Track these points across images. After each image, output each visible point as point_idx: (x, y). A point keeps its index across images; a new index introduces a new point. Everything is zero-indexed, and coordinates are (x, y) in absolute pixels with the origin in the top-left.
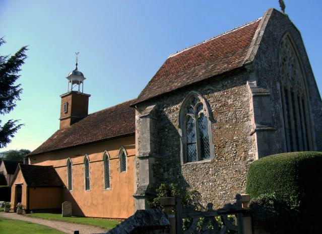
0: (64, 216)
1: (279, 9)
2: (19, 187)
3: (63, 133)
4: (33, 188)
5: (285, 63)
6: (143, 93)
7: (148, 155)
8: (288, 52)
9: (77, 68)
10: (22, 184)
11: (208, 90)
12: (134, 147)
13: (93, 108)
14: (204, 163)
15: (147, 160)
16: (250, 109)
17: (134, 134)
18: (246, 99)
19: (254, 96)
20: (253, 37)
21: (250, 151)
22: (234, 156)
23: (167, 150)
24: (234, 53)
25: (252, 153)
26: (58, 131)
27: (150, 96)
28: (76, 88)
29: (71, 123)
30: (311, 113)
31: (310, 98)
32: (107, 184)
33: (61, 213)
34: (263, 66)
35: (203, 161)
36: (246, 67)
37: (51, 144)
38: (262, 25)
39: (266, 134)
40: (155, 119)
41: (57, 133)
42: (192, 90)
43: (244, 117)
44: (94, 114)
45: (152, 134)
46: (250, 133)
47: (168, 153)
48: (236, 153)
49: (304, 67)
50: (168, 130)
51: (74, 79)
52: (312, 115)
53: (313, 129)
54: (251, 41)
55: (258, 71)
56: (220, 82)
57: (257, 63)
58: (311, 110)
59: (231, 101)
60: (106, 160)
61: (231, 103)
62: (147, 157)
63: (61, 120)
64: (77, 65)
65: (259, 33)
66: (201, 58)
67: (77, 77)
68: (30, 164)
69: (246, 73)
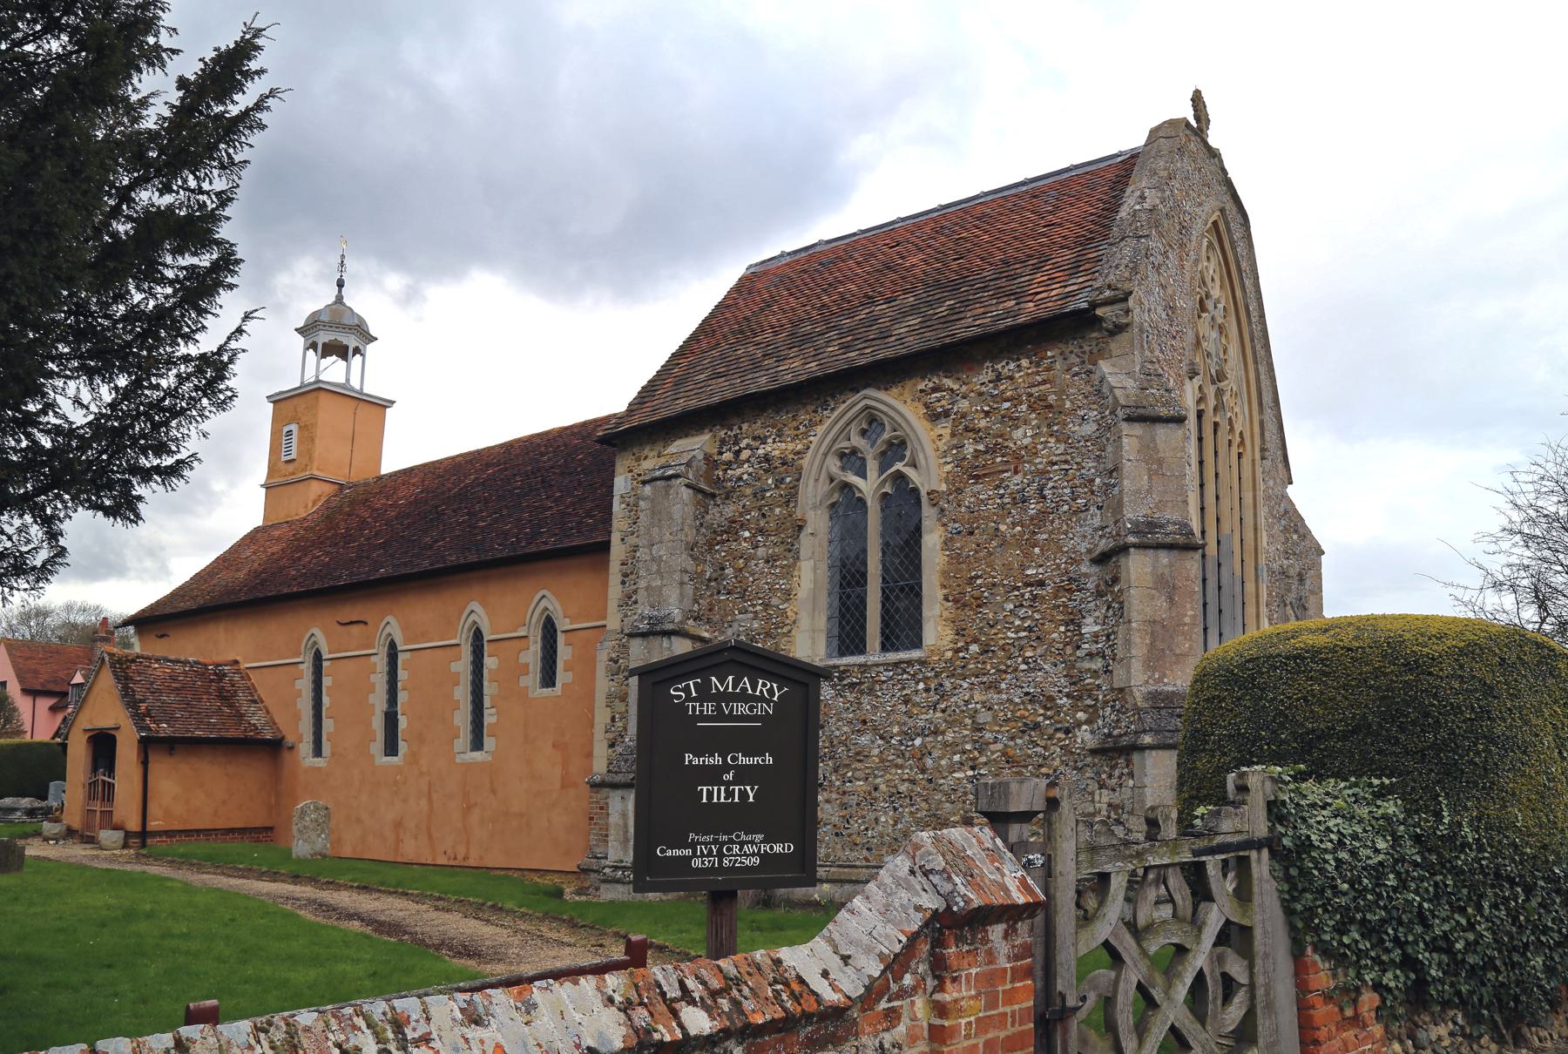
10: (117, 729)
11: (935, 390)
14: (897, 664)
17: (605, 547)
20: (260, 876)
21: (1089, 620)
23: (744, 611)
25: (1097, 628)
26: (257, 530)
27: (681, 405)
30: (1260, 501)
35: (892, 657)
37: (226, 577)
39: (1164, 558)
41: (252, 537)
50: (754, 536)
53: (1262, 561)
56: (987, 364)
58: (1260, 494)
59: (1025, 436)
61: (1026, 441)
66: (894, 276)
67: (166, 103)
69: (1095, 335)
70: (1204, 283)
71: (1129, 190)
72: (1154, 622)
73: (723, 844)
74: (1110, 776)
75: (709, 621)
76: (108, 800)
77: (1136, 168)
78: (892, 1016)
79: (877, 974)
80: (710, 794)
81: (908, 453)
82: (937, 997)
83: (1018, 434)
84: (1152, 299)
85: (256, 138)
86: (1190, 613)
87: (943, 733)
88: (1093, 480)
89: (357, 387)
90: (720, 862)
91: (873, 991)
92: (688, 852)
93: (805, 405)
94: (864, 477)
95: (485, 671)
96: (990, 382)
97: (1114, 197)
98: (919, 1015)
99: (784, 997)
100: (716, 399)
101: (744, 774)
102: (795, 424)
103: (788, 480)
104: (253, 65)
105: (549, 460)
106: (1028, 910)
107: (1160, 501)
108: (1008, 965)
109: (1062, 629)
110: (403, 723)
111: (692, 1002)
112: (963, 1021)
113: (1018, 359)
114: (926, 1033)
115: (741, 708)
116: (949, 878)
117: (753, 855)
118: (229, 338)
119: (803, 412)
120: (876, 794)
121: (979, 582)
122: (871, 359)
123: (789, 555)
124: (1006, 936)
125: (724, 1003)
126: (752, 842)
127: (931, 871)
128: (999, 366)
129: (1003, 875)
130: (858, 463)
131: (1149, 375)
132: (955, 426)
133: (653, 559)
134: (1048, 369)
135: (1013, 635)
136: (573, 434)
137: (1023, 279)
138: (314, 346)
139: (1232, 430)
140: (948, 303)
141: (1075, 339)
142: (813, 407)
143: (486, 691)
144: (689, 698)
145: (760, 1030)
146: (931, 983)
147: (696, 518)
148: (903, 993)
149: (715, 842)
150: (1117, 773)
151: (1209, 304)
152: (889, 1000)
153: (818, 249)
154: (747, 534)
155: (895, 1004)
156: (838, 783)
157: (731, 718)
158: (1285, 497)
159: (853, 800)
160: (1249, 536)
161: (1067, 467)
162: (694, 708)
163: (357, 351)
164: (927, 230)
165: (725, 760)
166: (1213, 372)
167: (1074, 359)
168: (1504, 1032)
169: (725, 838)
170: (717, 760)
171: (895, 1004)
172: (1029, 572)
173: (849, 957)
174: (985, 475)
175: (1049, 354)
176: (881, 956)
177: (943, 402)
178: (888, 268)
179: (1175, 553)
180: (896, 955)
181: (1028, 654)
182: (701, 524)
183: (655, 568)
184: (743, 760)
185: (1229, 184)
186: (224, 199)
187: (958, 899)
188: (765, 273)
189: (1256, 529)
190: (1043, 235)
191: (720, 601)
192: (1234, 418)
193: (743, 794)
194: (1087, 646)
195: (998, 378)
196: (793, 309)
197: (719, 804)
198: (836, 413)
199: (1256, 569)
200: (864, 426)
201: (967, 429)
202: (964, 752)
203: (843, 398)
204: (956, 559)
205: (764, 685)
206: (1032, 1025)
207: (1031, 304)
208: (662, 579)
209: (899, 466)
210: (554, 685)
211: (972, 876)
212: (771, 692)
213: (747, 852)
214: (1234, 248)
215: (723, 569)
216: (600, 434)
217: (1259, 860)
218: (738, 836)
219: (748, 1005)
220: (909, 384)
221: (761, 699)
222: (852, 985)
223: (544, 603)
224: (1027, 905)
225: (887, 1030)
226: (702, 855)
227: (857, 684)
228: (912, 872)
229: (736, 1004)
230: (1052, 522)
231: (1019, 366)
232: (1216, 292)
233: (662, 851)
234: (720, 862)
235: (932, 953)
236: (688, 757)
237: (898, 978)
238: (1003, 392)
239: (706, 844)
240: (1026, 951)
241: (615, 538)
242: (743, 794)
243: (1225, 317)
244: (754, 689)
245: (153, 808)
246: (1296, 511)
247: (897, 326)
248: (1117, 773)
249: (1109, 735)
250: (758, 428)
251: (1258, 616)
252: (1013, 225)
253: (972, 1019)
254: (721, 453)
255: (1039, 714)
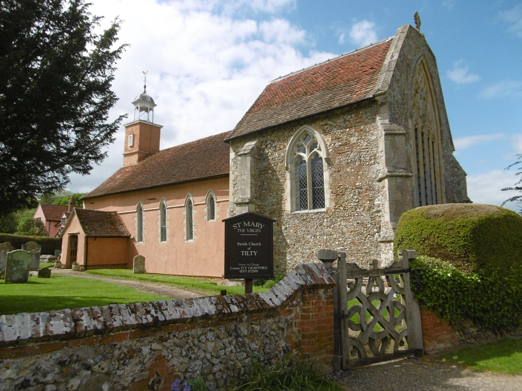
0: (135, 273)
1: (414, 26)
2: (74, 238)
3: (128, 172)
4: (93, 239)
5: (417, 95)
6: (240, 124)
7: (248, 201)
8: (421, 81)
9: (145, 91)
10: (79, 233)
11: (326, 125)
12: (227, 194)
13: (164, 145)
14: (317, 213)
15: (247, 207)
16: (379, 150)
17: (228, 175)
18: (374, 138)
19: (386, 135)
21: (377, 200)
22: (356, 205)
23: (271, 196)
24: (358, 79)
25: (379, 202)
26: (121, 169)
28: (144, 116)
29: (140, 160)
30: (441, 158)
31: (442, 140)
32: (190, 235)
33: (132, 269)
34: (396, 98)
35: (316, 211)
36: (376, 98)
38: (396, 46)
39: (399, 180)
40: (256, 158)
42: (305, 124)
43: (370, 160)
44: (168, 150)
45: (253, 176)
46: (377, 179)
47: (271, 200)
48: (358, 202)
49: (437, 102)
51: (143, 105)
52: (443, 161)
53: (443, 178)
54: (381, 67)
55: (391, 104)
56: (342, 116)
57: (390, 94)
58: (441, 155)
60: (189, 206)
61: (355, 141)
62: (247, 203)
63: (125, 155)
64: (145, 87)
65: (392, 56)
66: (314, 85)
68: (84, 208)
69: (375, 106)
70: (417, 83)
71: (388, 53)
72: (397, 201)
73: (248, 266)
74: (385, 250)
75: (260, 199)
76: (74, 255)
77: (392, 45)
78: (290, 312)
79: (285, 300)
80: (244, 253)
81: (318, 146)
82: (303, 307)
83: (352, 139)
84: (395, 92)
85: (117, 60)
86: (409, 198)
87: (333, 235)
88: (376, 155)
89: (151, 122)
90: (247, 271)
91: (284, 305)
92: (238, 268)
93: (286, 130)
94: (305, 153)
95: (193, 214)
96: (343, 122)
97: (384, 55)
98: (298, 312)
99: (258, 304)
100: (259, 128)
101: (253, 248)
102: (284, 136)
103: (282, 154)
104: (115, 37)
105: (211, 146)
106: (332, 286)
107: (397, 161)
108: (325, 301)
109: (368, 202)
110: (168, 231)
111: (233, 304)
112: (311, 314)
113: (351, 114)
114: (300, 317)
115: (252, 231)
116: (306, 276)
117: (256, 269)
118: (115, 122)
119: (286, 132)
120: (313, 254)
121: (342, 187)
122: (306, 115)
123: (283, 178)
124: (324, 292)
125: (242, 305)
126: (256, 266)
127: (302, 274)
128: (345, 117)
129: (323, 276)
130: (303, 149)
131: (393, 119)
132: (332, 137)
133: (242, 180)
134: (361, 118)
135: (353, 204)
136: (218, 138)
137: (353, 86)
138: (137, 108)
139: (429, 134)
140: (330, 95)
141: (369, 107)
142: (289, 131)
143: (193, 221)
144: (238, 228)
145: (252, 312)
146: (302, 304)
147: (255, 167)
148: (293, 306)
149: (246, 266)
150: (387, 248)
151: (420, 90)
152: (289, 307)
153: (291, 75)
154: (270, 172)
155: (291, 308)
156: (301, 250)
157: (249, 233)
158: (451, 156)
159: (306, 255)
160: (437, 170)
161: (368, 150)
162: (239, 230)
163: (151, 109)
164: (324, 68)
165: (248, 244)
166: (421, 114)
167: (369, 114)
168: (497, 331)
169: (249, 265)
170: (246, 244)
171: (291, 308)
172: (357, 184)
173: (277, 295)
174: (342, 153)
175: (361, 112)
176: (286, 295)
177: (328, 129)
178: (312, 82)
179: (403, 178)
180: (290, 296)
181: (358, 210)
182: (256, 168)
183: (243, 183)
184: (253, 244)
185: (427, 46)
186: (111, 78)
187: (308, 282)
188: (275, 84)
189: (440, 168)
190: (360, 70)
191: (263, 193)
192: (430, 130)
193: (253, 253)
194: (376, 208)
195: (345, 121)
196: (283, 97)
197: (247, 256)
198: (296, 133)
199: (441, 181)
200: (305, 137)
201: (336, 138)
202: (339, 241)
203: (298, 128)
204: (335, 180)
205: (258, 224)
206: (333, 317)
207: (355, 95)
208: (245, 186)
209: (315, 150)
210: (214, 218)
211: (313, 276)
212: (260, 226)
213: (254, 269)
214: (429, 70)
215: (264, 183)
216: (225, 139)
217: (406, 276)
218: (252, 264)
219: (248, 306)
220: (318, 123)
221: (257, 228)
222: (277, 302)
223: (210, 193)
224: (330, 285)
225: (288, 315)
226: (242, 269)
227: (305, 219)
228: (297, 274)
229: (245, 305)
230: (364, 168)
231: (351, 117)
232: (422, 85)
233: (232, 268)
234: (247, 271)
235: (302, 296)
236: (238, 243)
237: (292, 302)
238: (347, 125)
239: (243, 266)
240: (331, 297)
241: (231, 173)
242: (253, 253)
243: (426, 94)
244: (255, 225)
245: (89, 258)
246: (456, 161)
247: (314, 103)
248: (387, 248)
249: (384, 237)
250: (272, 137)
251: (442, 197)
252: (351, 67)
253: (314, 314)
254: (262, 146)
255: (361, 229)
